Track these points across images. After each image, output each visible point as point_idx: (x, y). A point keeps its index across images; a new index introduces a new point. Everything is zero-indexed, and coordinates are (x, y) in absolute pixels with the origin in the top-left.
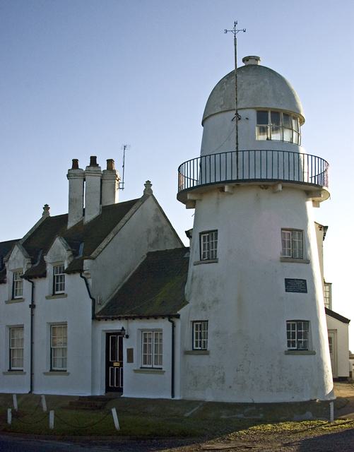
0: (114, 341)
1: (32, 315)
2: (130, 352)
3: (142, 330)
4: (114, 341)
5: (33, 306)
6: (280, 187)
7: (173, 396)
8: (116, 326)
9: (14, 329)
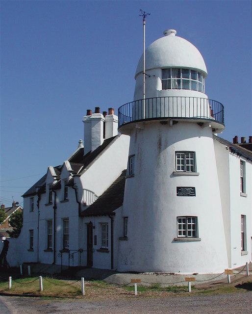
0: (90, 227)
1: (55, 213)
2: (96, 236)
3: (101, 223)
4: (90, 227)
5: (55, 208)
6: (171, 123)
7: (112, 269)
8: (87, 220)
9: (49, 222)
